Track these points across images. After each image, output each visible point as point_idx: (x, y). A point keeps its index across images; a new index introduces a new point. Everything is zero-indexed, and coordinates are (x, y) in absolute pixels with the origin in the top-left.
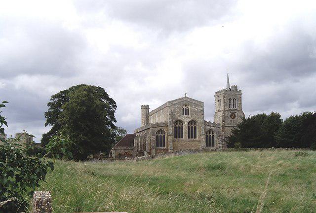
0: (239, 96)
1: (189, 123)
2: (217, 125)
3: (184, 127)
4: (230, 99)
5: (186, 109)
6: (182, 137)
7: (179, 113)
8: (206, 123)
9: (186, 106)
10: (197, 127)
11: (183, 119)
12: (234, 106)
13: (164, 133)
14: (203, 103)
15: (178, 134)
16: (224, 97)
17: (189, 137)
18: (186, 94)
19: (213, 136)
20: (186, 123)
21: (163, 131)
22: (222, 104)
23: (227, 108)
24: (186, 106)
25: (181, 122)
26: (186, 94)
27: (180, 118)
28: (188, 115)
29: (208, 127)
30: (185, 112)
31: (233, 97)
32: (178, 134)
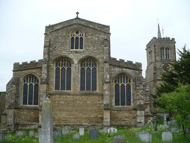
0: (173, 45)
1: (82, 62)
2: (134, 65)
3: (73, 69)
4: (162, 49)
5: (77, 38)
6: (69, 88)
7: (63, 44)
8: (114, 63)
9: (77, 33)
10: (97, 69)
11: (71, 56)
12: (167, 55)
13: (36, 80)
14: (108, 27)
15: (63, 82)
16: (155, 46)
17: (82, 88)
18: (77, 13)
19: (128, 86)
20: (76, 62)
21: (36, 78)
22: (153, 54)
23: (158, 58)
24: (77, 33)
25: (69, 61)
26: (77, 13)
27: (64, 53)
28: (81, 48)
29: (117, 70)
30: (77, 43)
31: (166, 46)
32: (63, 82)
